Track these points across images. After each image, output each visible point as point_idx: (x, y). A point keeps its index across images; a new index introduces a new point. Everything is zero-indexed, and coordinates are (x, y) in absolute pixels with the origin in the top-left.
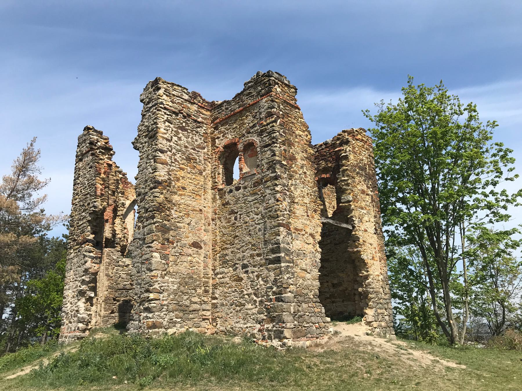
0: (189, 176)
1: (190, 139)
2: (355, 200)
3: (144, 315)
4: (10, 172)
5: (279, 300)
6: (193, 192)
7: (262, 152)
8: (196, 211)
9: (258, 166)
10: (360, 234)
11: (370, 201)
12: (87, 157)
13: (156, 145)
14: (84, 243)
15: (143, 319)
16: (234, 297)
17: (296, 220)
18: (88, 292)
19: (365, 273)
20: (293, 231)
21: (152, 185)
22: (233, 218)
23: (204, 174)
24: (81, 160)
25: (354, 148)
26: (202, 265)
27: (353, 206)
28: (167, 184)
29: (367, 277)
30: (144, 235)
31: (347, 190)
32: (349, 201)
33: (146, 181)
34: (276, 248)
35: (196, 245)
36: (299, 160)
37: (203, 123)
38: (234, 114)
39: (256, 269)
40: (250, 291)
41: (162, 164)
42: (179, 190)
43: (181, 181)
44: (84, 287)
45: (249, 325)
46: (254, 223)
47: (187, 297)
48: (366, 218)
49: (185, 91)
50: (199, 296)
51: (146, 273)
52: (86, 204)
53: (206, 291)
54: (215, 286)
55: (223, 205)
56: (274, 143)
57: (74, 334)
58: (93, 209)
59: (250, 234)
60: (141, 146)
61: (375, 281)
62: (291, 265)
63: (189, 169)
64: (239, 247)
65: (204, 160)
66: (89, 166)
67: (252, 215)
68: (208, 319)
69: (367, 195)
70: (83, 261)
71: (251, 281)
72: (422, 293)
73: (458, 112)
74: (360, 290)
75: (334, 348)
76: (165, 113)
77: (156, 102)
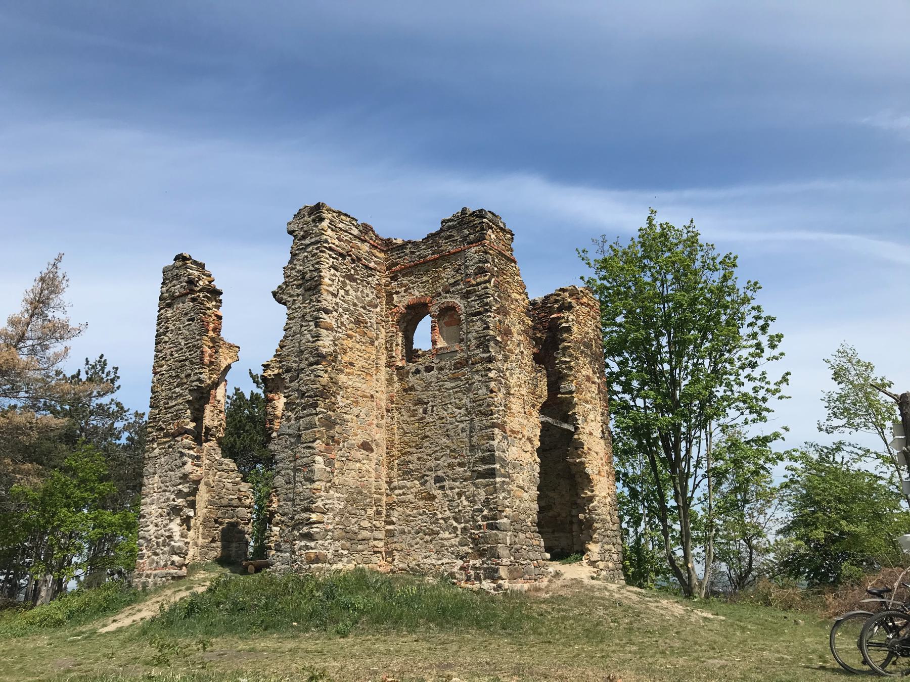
0: (358, 346)
1: (359, 293)
2: (579, 390)
3: (299, 543)
4: (17, 307)
5: (492, 527)
6: (363, 370)
7: (468, 323)
8: (367, 397)
9: (462, 340)
10: (584, 438)
11: (596, 392)
12: (184, 303)
13: (319, 301)
14: (181, 434)
15: (300, 549)
16: (422, 522)
17: (512, 419)
18: (185, 510)
19: (589, 493)
20: (509, 433)
21: (312, 359)
22: (421, 410)
23: (376, 343)
24: (169, 306)
25: (578, 316)
26: (373, 474)
27: (576, 399)
28: (330, 359)
29: (591, 499)
30: (299, 430)
31: (569, 375)
32: (572, 392)
33: (302, 352)
34: (488, 456)
35: (366, 446)
36: (515, 335)
37: (375, 269)
38: (424, 262)
39: (457, 484)
40: (448, 514)
41: (327, 329)
42: (346, 367)
43: (348, 354)
44: (180, 501)
45: (445, 561)
46: (454, 420)
47: (355, 520)
48: (591, 417)
49: (354, 222)
50: (369, 518)
51: (303, 485)
52: (183, 375)
53: (378, 513)
54: (391, 506)
55: (405, 390)
56: (487, 311)
57: (165, 571)
58: (197, 383)
59: (448, 435)
60: (289, 299)
61: (602, 505)
62: (507, 480)
63: (358, 337)
64: (430, 451)
65: (377, 323)
66: (188, 317)
67: (451, 408)
68: (380, 552)
69: (594, 383)
70: (179, 462)
71: (449, 501)
72: (637, 523)
73: (711, 267)
74: (581, 516)
75: (562, 592)
76: (330, 256)
77: (318, 238)
